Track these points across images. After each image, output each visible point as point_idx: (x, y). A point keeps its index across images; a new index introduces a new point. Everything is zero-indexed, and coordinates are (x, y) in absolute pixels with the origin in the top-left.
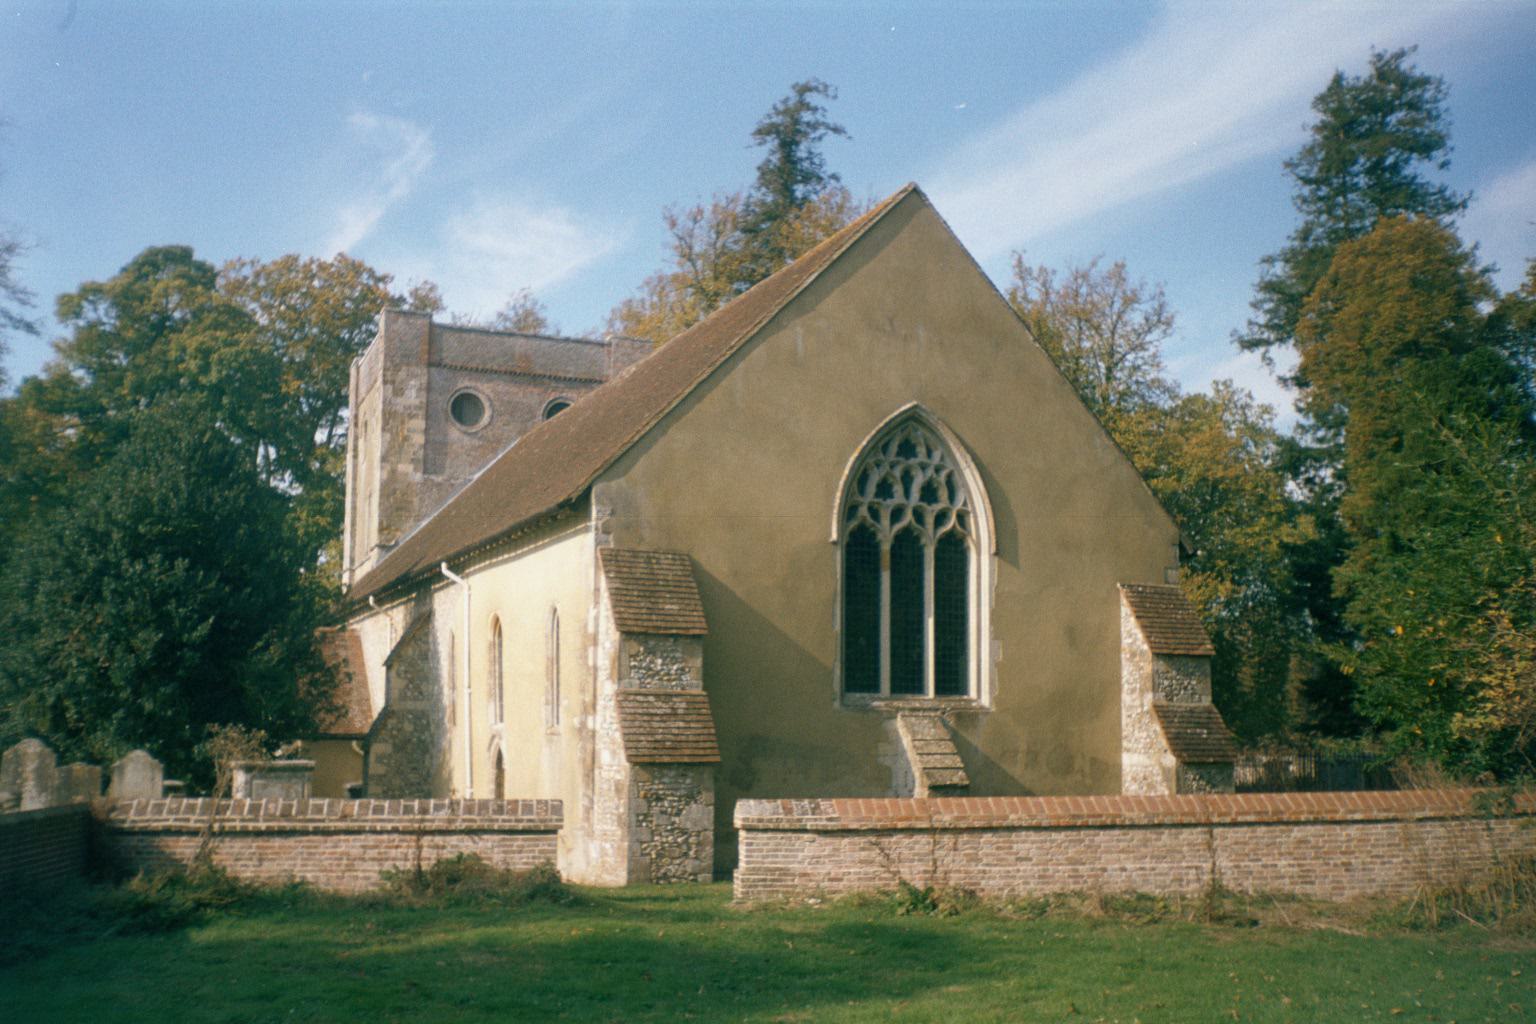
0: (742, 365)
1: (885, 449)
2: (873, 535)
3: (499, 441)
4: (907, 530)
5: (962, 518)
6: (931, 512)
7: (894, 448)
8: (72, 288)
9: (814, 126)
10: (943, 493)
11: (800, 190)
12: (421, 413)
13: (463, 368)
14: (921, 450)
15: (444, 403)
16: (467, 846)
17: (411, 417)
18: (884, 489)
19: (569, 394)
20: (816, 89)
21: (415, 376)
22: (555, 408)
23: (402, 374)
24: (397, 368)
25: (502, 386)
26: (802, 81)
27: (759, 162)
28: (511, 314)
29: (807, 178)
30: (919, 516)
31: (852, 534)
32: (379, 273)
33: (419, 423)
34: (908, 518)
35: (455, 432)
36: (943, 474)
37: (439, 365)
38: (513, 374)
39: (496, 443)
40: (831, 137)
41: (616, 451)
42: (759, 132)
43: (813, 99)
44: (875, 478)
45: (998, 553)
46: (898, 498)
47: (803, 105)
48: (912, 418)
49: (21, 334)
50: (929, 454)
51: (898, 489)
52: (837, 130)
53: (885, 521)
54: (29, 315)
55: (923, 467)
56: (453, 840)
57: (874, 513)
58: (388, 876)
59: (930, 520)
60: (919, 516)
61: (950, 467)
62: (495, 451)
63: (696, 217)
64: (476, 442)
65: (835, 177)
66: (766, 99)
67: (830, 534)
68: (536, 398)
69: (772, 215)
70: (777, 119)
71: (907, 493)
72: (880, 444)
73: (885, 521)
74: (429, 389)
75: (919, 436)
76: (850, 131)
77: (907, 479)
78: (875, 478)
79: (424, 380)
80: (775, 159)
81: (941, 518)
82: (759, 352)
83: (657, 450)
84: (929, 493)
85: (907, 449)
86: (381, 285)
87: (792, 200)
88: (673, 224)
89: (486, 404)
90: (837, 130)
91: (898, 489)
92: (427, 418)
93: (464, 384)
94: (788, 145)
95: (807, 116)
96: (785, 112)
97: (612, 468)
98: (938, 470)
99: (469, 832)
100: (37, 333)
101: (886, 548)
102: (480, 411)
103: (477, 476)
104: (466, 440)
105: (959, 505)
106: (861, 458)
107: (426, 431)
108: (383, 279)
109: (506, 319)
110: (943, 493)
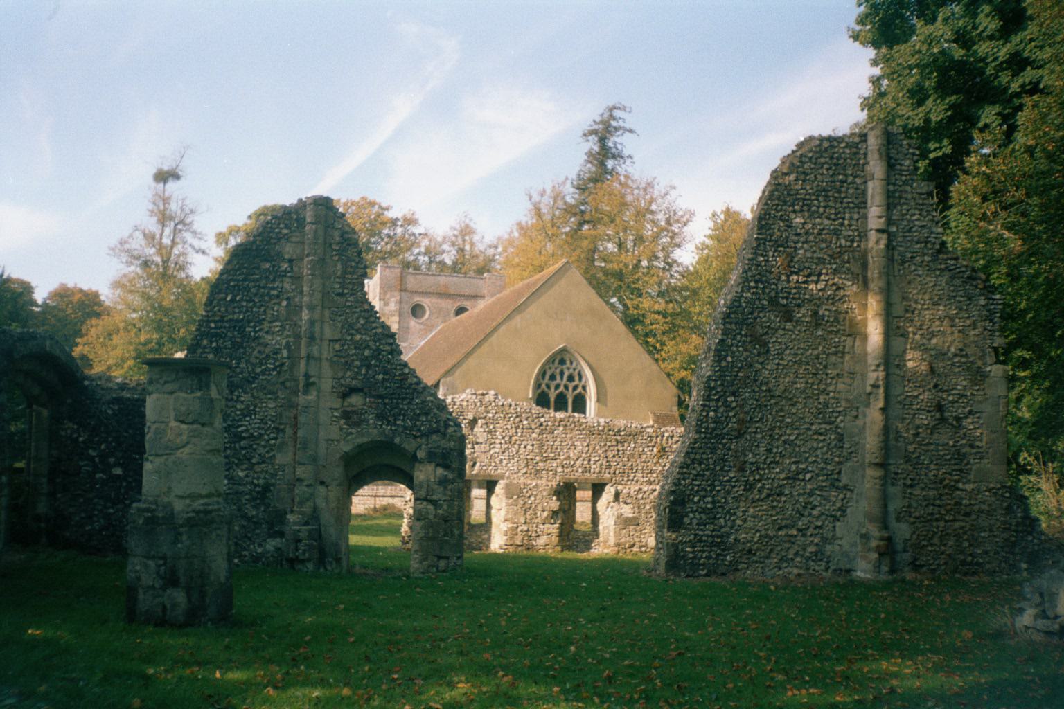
0: (495, 335)
1: (553, 362)
2: (547, 395)
3: (433, 326)
4: (561, 393)
5: (584, 388)
6: (571, 385)
7: (557, 362)
8: (224, 229)
9: (616, 129)
10: (577, 378)
11: (610, 164)
12: (397, 314)
13: (416, 292)
14: (568, 362)
15: (407, 308)
16: (391, 500)
17: (392, 315)
18: (553, 377)
19: (466, 304)
20: (619, 108)
21: (394, 296)
22: (460, 311)
23: (388, 296)
24: (385, 293)
25: (434, 300)
26: (611, 105)
27: (586, 150)
28: (458, 227)
29: (614, 157)
30: (566, 387)
31: (539, 395)
32: (384, 205)
33: (396, 318)
34: (562, 388)
35: (413, 323)
36: (577, 371)
37: (405, 290)
38: (438, 294)
39: (433, 326)
40: (627, 134)
41: (450, 366)
42: (585, 135)
43: (617, 113)
44: (549, 373)
45: (598, 400)
46: (558, 380)
47: (612, 117)
48: (564, 350)
49: (200, 256)
50: (571, 363)
51: (558, 377)
52: (631, 131)
53: (553, 389)
54: (203, 246)
55: (568, 369)
56: (386, 499)
57: (548, 386)
58: (366, 509)
59: (571, 389)
60: (566, 387)
61: (579, 368)
62: (431, 331)
63: (543, 194)
64: (422, 327)
65: (630, 157)
66: (589, 114)
67: (528, 394)
68: (451, 306)
69: (595, 180)
70: (596, 127)
71: (562, 379)
72: (551, 360)
73: (553, 389)
74: (401, 302)
75: (567, 357)
76: (638, 132)
77: (562, 373)
78: (549, 373)
79: (398, 298)
80: (596, 148)
81: (575, 388)
82: (503, 328)
83: (464, 367)
84: (571, 378)
85: (562, 362)
86: (386, 213)
87: (606, 172)
88: (530, 198)
89: (427, 309)
90: (631, 131)
91: (558, 377)
92: (400, 315)
93: (417, 299)
94: (602, 140)
95: (614, 123)
96: (602, 122)
97: (447, 373)
98: (574, 369)
99: (391, 496)
100: (208, 255)
101: (552, 399)
102: (424, 312)
103: (423, 343)
104: (418, 326)
105: (583, 382)
106: (544, 365)
107: (399, 322)
108: (387, 209)
109: (455, 229)
110: (577, 378)
